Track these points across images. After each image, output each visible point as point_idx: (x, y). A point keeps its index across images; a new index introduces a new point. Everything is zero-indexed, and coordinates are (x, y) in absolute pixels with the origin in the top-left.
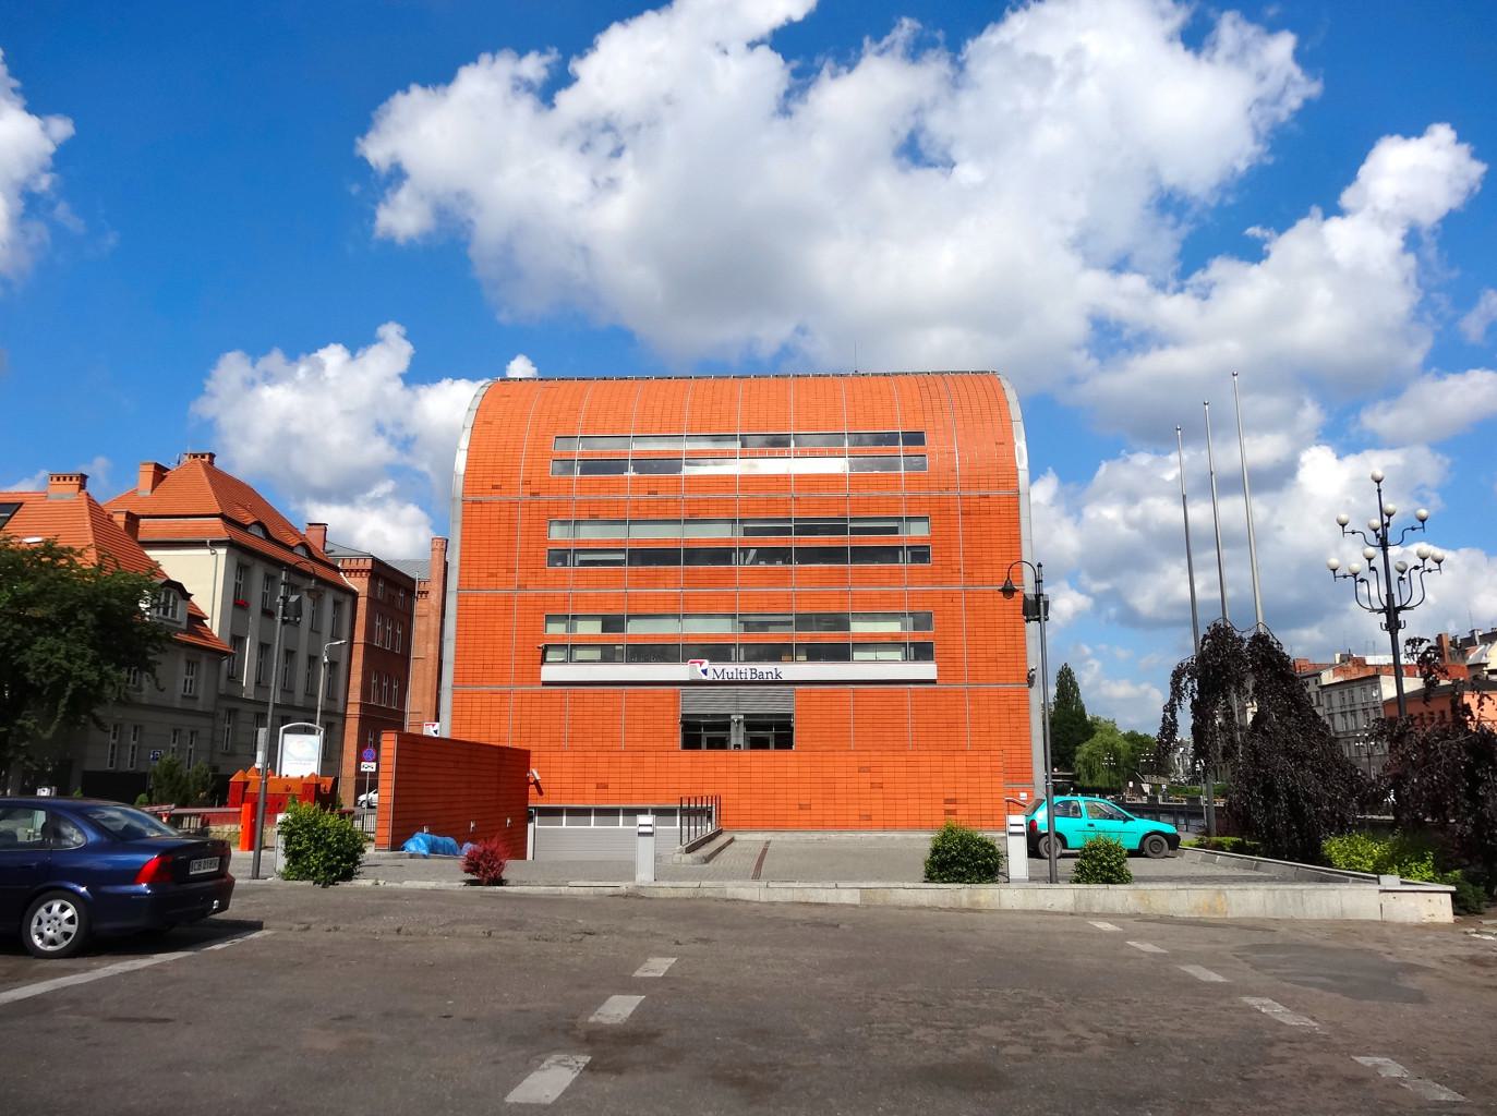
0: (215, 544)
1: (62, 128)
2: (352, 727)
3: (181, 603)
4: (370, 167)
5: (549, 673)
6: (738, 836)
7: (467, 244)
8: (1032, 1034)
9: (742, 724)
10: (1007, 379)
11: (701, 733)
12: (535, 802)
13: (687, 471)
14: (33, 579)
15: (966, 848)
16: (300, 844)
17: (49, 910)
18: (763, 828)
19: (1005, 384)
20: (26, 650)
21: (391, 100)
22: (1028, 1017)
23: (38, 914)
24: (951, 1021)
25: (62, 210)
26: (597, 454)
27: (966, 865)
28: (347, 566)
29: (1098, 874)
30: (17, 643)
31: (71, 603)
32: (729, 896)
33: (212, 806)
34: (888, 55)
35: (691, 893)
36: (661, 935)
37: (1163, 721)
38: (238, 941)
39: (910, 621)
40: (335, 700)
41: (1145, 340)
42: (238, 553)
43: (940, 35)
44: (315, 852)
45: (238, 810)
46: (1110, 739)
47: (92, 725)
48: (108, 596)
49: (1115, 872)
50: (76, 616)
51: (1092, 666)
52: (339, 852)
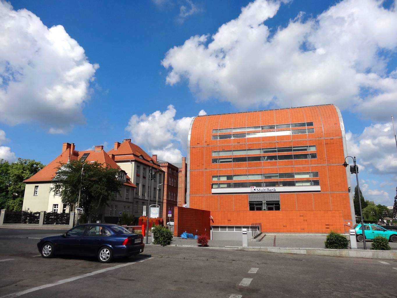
0: (132, 161)
1: (97, 66)
2: (165, 205)
3: (125, 176)
4: (165, 68)
5: (214, 191)
6: (267, 234)
7: (188, 84)
8: (371, 295)
9: (266, 204)
10: (337, 106)
11: (255, 206)
12: (212, 224)
13: (247, 137)
14: (93, 171)
15: (337, 239)
16: (157, 235)
17: (103, 251)
18: (273, 232)
19: (336, 107)
20: (92, 188)
21: (169, 50)
22: (368, 290)
23: (101, 252)
24: (344, 290)
25: (97, 85)
26: (228, 133)
27: (338, 243)
28: (162, 165)
29: (379, 247)
30: (90, 186)
31: (101, 176)
32: (269, 251)
33: (135, 225)
34: (296, 23)
35: (258, 250)
36: (253, 262)
37: (395, 201)
38: (146, 260)
39: (312, 174)
40: (161, 199)
41: (377, 92)
42: (137, 163)
43: (311, 14)
44: (161, 237)
45: (141, 226)
46: (372, 207)
47: (106, 206)
48: (109, 174)
49: (385, 246)
50: (102, 179)
51: (365, 186)
52: (167, 237)
